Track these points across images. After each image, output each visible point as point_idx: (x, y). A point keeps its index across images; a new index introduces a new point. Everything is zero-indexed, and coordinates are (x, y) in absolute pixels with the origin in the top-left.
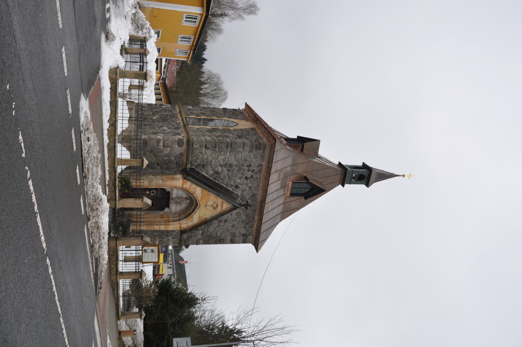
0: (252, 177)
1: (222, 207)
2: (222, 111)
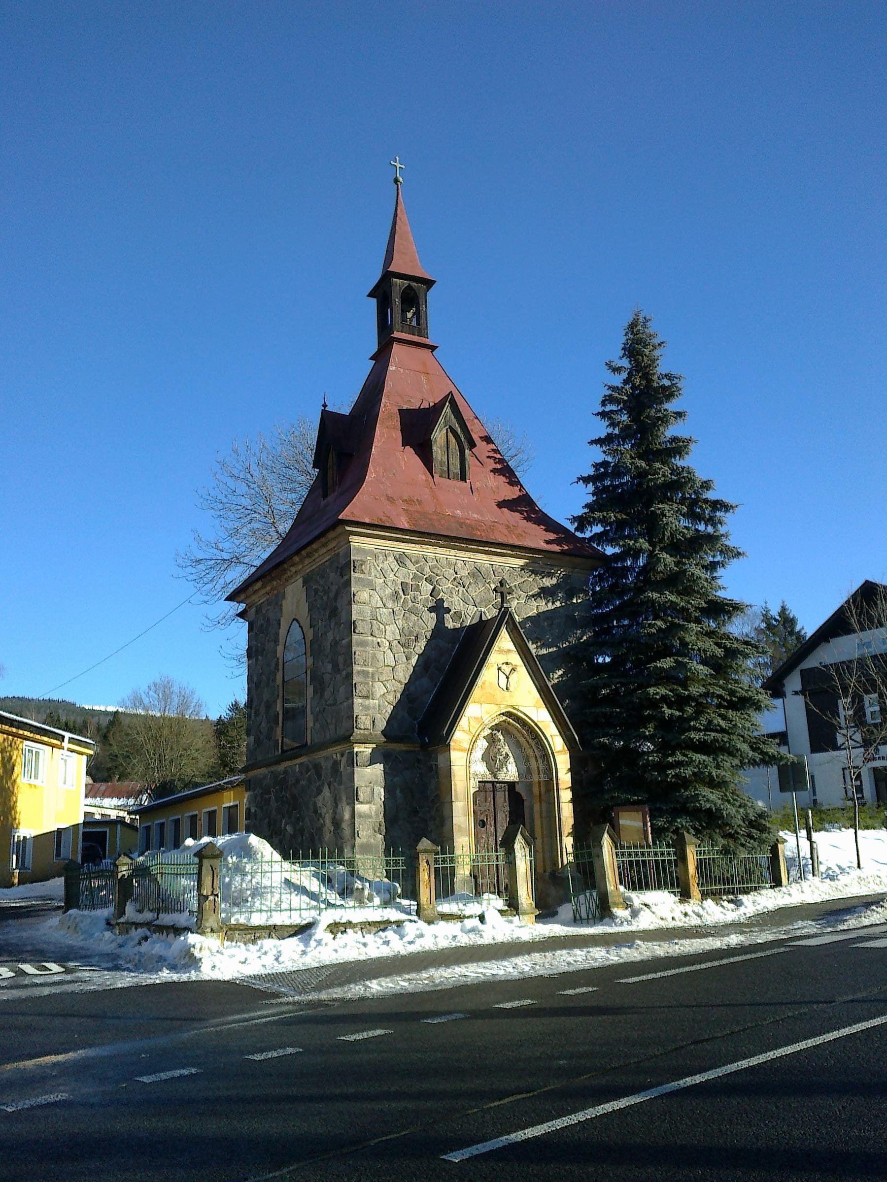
0: (429, 580)
2: (257, 660)
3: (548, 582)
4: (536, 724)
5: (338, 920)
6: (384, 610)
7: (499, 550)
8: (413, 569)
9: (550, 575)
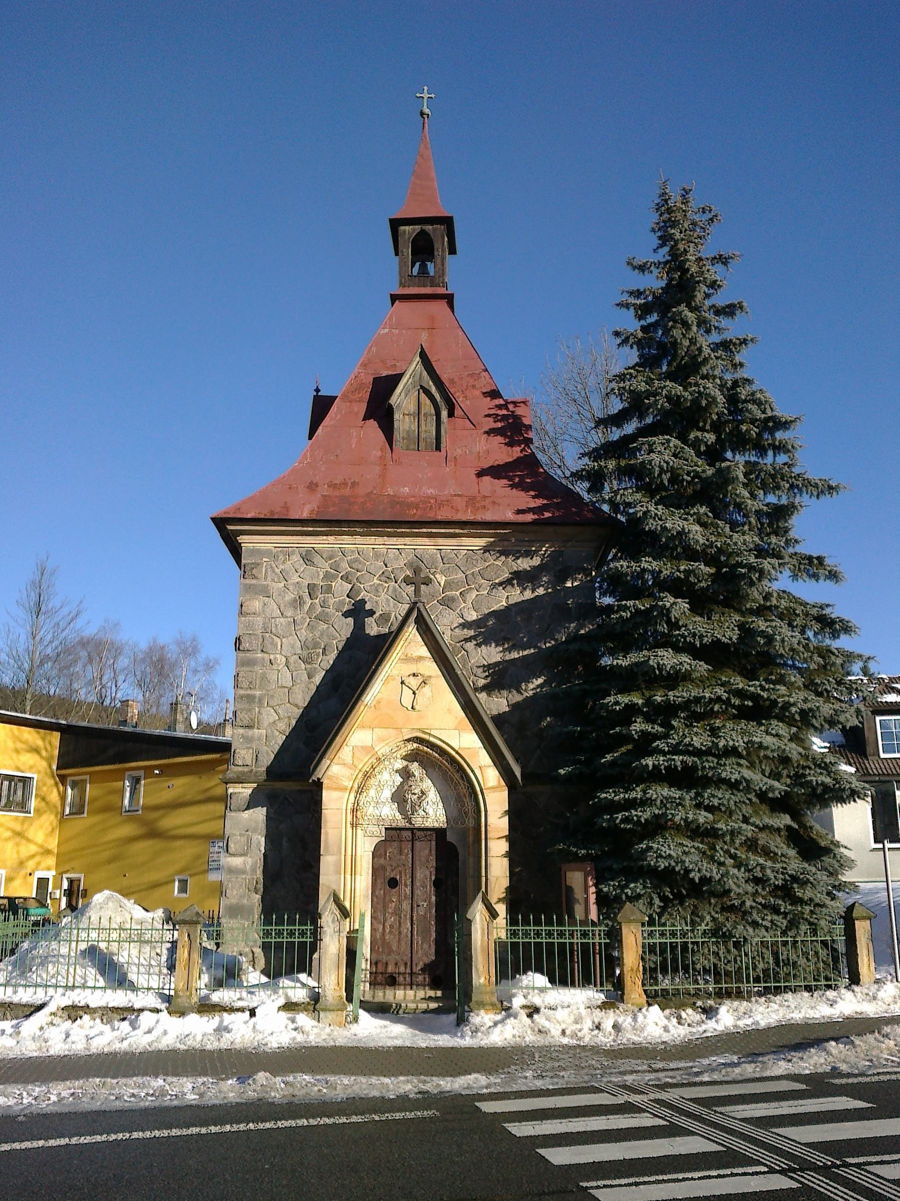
0: (345, 578)
1: (421, 658)
3: (524, 564)
4: (457, 753)
5: (76, 1003)
6: (282, 620)
7: (443, 531)
8: (326, 566)
9: (529, 554)
